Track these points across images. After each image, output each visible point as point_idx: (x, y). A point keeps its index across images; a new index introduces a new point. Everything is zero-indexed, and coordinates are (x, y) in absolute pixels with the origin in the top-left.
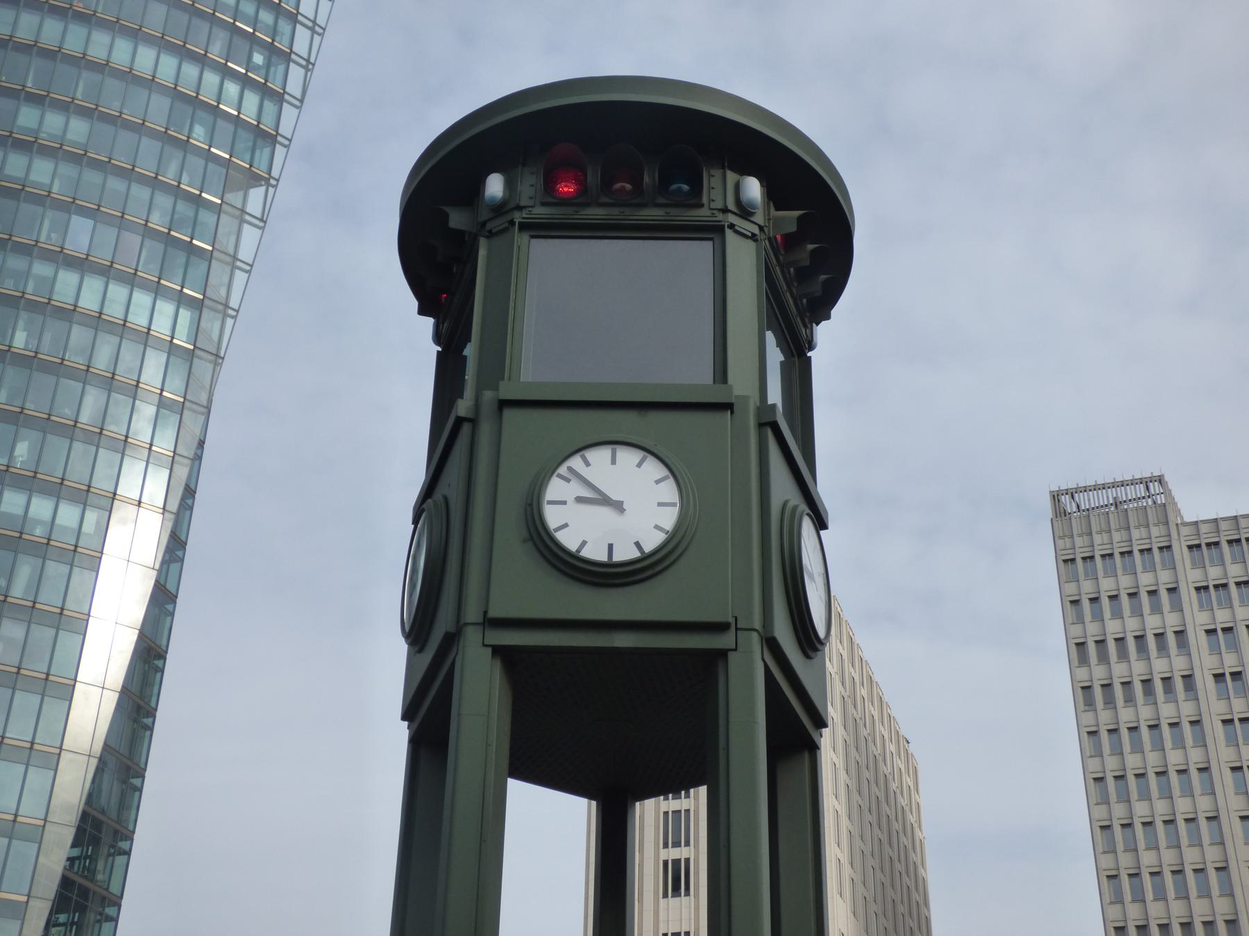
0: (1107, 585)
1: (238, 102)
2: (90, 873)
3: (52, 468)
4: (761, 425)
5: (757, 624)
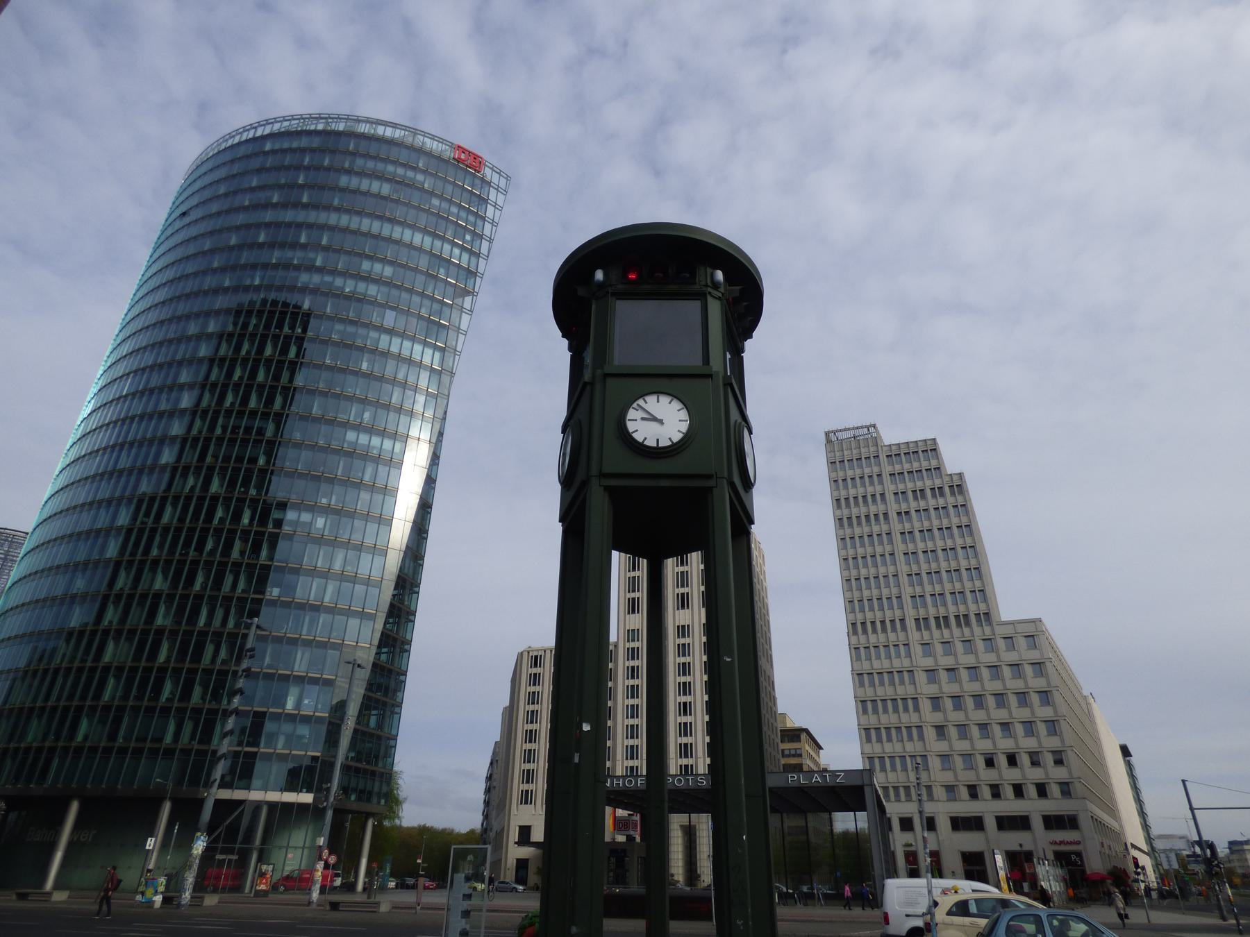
0: (850, 473)
1: (456, 256)
2: (402, 601)
3: (380, 425)
4: (725, 385)
5: (726, 475)
